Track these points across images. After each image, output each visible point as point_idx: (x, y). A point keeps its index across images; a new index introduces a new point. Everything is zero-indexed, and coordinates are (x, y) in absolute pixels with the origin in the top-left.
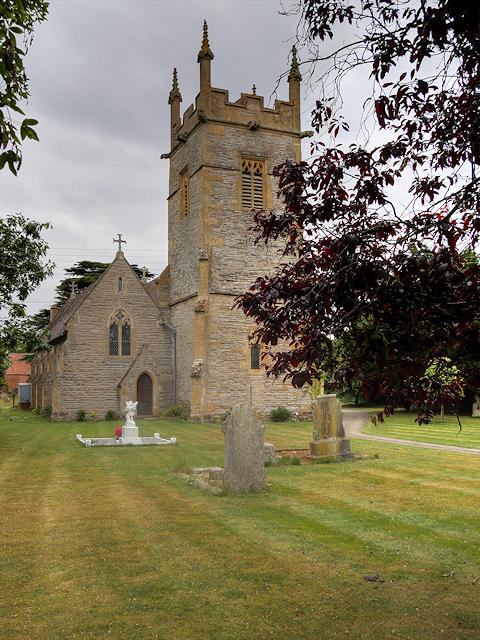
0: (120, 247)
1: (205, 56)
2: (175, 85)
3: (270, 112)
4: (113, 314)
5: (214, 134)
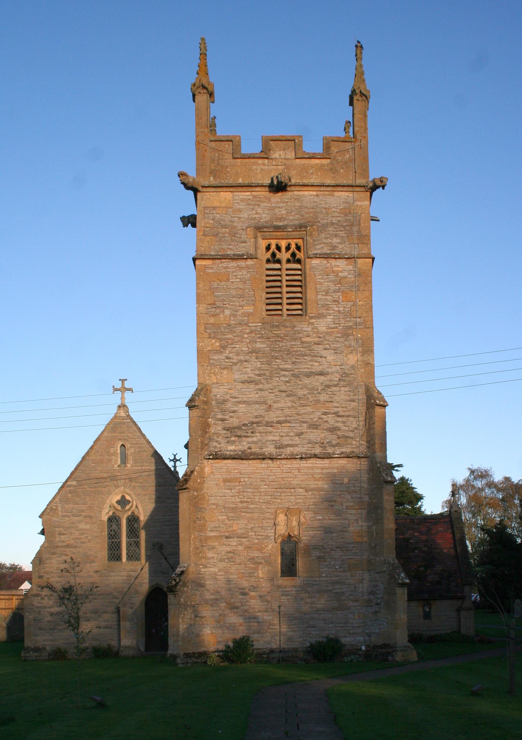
0: (123, 398)
5: (215, 208)
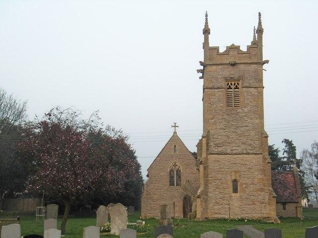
1: (206, 32)
2: (207, 23)
3: (244, 53)
4: (171, 164)
